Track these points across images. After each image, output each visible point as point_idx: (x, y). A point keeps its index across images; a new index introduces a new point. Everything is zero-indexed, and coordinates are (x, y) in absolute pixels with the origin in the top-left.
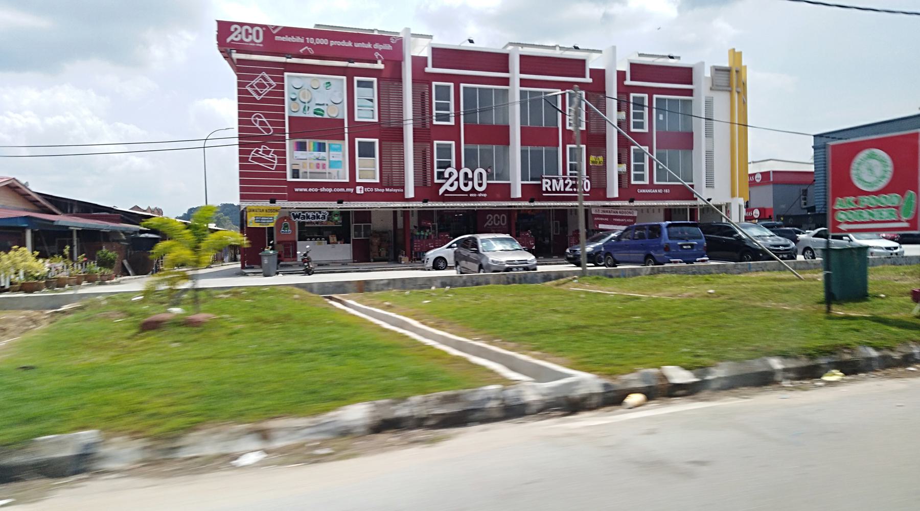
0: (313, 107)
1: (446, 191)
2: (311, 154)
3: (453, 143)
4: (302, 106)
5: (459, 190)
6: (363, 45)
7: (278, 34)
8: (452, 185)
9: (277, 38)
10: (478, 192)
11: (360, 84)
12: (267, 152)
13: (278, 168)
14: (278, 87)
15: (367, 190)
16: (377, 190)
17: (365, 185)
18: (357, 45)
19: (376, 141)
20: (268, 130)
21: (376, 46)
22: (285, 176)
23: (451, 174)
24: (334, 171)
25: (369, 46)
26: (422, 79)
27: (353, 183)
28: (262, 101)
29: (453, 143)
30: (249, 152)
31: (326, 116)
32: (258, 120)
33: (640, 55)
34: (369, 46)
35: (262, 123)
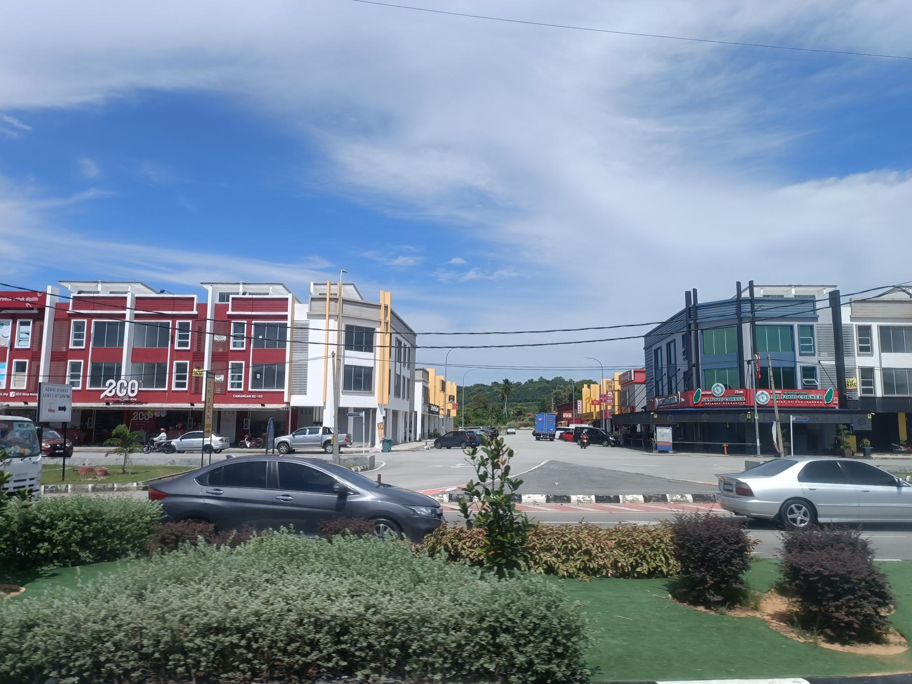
1: (106, 396)
3: (82, 361)
5: (115, 395)
8: (111, 392)
10: (130, 397)
11: (22, 324)
15: (17, 394)
16: (24, 394)
19: (27, 361)
21: (28, 299)
23: (111, 384)
27: (8, 390)
29: (82, 361)
33: (111, 293)
34: (23, 299)
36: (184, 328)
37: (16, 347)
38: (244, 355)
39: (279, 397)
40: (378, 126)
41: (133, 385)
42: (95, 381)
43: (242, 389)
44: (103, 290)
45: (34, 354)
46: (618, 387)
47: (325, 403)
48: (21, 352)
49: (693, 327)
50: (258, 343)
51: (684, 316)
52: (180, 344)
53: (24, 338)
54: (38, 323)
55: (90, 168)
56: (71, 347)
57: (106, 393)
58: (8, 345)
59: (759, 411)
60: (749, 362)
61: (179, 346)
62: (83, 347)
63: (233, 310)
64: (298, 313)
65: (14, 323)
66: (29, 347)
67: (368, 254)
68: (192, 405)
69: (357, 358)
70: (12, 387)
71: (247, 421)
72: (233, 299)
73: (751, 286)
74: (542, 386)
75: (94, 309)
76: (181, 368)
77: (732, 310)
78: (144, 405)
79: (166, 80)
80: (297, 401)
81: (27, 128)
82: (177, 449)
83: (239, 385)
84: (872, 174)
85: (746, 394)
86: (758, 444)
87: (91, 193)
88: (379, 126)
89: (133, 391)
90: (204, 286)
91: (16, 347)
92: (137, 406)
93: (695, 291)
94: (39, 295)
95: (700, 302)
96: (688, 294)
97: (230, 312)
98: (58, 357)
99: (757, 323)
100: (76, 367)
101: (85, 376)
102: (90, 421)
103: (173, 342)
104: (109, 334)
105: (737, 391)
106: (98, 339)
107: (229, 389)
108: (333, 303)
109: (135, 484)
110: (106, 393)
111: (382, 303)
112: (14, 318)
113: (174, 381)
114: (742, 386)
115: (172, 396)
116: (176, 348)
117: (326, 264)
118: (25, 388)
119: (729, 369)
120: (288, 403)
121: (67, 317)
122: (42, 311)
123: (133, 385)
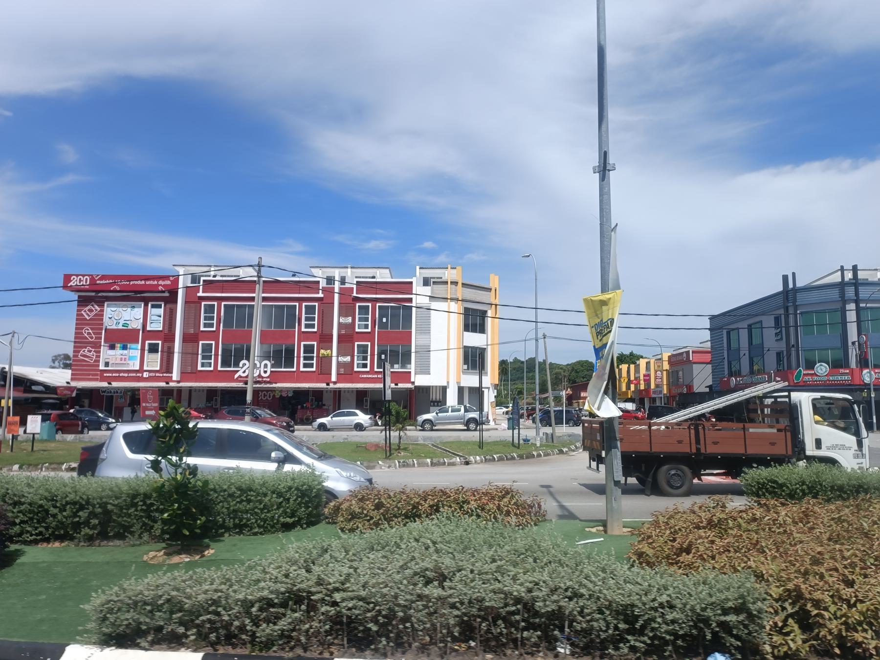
0: (122, 322)
1: (240, 377)
2: (118, 352)
3: (213, 342)
4: (115, 322)
6: (151, 282)
7: (99, 279)
8: (244, 372)
9: (98, 282)
10: (263, 377)
11: (153, 306)
12: (90, 351)
13: (95, 361)
14: (80, 311)
15: (151, 374)
16: (157, 375)
17: (150, 371)
18: (148, 283)
19: (315, 343)
20: (92, 338)
21: (161, 282)
22: (98, 366)
24: (131, 362)
25: (156, 282)
26: (193, 301)
27: (141, 370)
28: (90, 320)
29: (213, 342)
30: (79, 352)
31: (130, 327)
32: (87, 331)
34: (156, 282)
35: (89, 334)
36: (310, 310)
37: (148, 329)
38: (369, 336)
39: (406, 377)
40: (354, 113)
41: (266, 366)
42: (225, 363)
43: (368, 369)
44: (383, 276)
45: (168, 336)
46: (666, 366)
47: (448, 382)
48: (154, 334)
49: (791, 311)
50: (382, 326)
51: (780, 301)
52: (307, 326)
53: (156, 319)
54: (168, 306)
55: (69, 153)
56: (202, 329)
57: (240, 373)
58: (140, 327)
59: (875, 390)
60: (853, 343)
61: (205, 327)
62: (214, 329)
63: (203, 292)
64: (420, 295)
65: (146, 305)
66: (161, 329)
67: (340, 238)
68: (396, 385)
69: (474, 340)
70: (145, 368)
71: (366, 401)
72: (204, 281)
73: (855, 269)
74: (516, 366)
75: (376, 294)
76: (309, 349)
77: (835, 294)
78: (274, 385)
79: (145, 67)
80: (420, 380)
81: (8, 114)
82: (329, 427)
83: (365, 366)
84: (826, 162)
85: (852, 373)
86: (875, 421)
87: (69, 179)
88: (353, 113)
89: (265, 372)
90: (176, 268)
91: (148, 329)
92: (268, 385)
93: (794, 274)
94: (171, 278)
95: (799, 284)
96: (785, 278)
97: (200, 294)
98: (190, 339)
99: (861, 305)
100: (207, 349)
101: (216, 355)
102: (216, 400)
103: (300, 324)
104: (238, 317)
105: (842, 371)
106: (228, 323)
107: (356, 369)
108: (453, 286)
109: (429, 460)
110: (240, 373)
111: (491, 285)
112: (146, 301)
113: (302, 361)
114: (847, 365)
115: (300, 376)
116: (303, 329)
117: (299, 248)
118: (158, 368)
119: (831, 349)
120: (413, 383)
121: (197, 300)
122: (174, 293)
123: (266, 366)
